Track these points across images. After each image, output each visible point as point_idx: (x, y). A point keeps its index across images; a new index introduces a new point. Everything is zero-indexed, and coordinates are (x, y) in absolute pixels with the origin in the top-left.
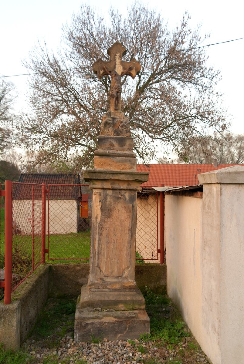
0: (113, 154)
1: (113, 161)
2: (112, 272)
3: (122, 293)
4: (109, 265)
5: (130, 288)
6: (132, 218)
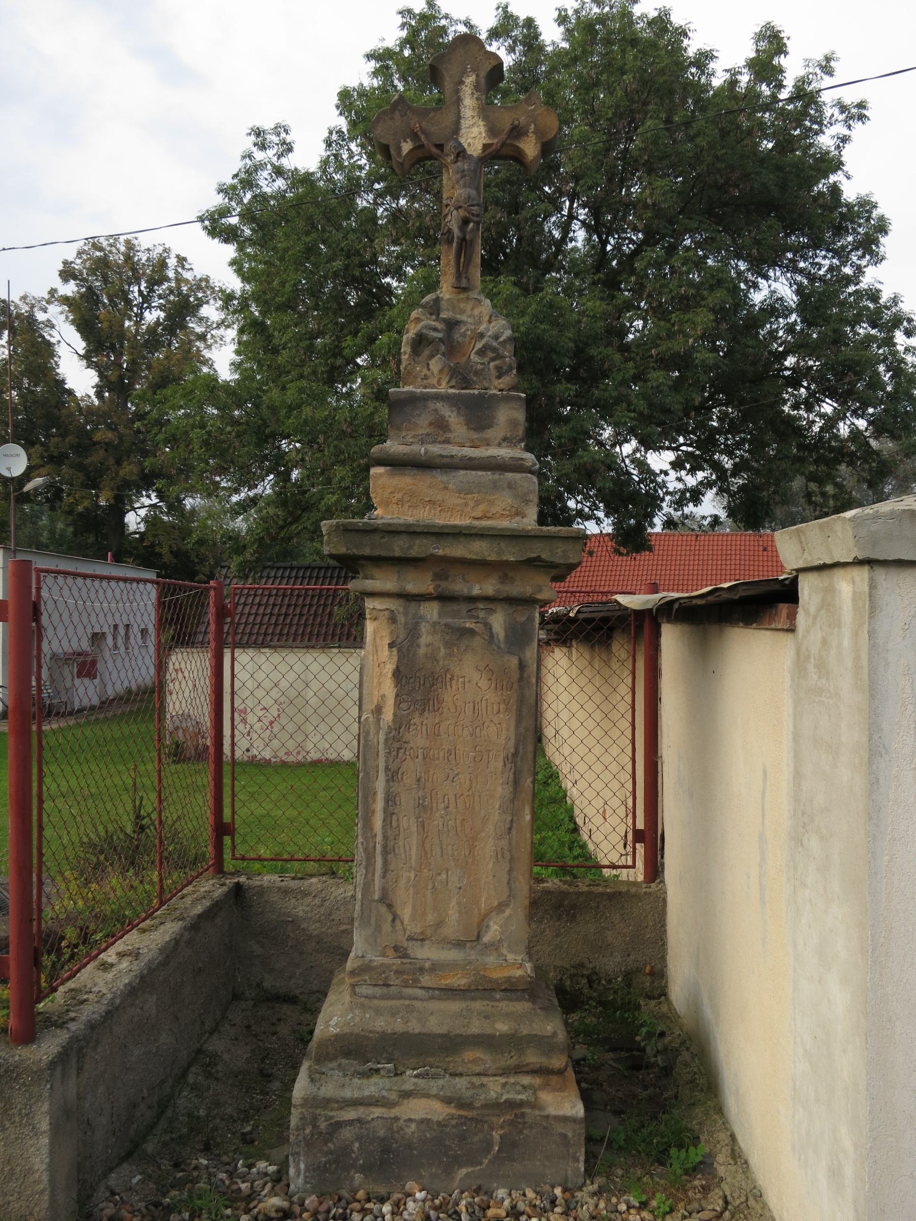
0: (445, 460)
1: (446, 488)
2: (439, 925)
3: (478, 1005)
4: (429, 896)
5: (511, 989)
6: (519, 710)
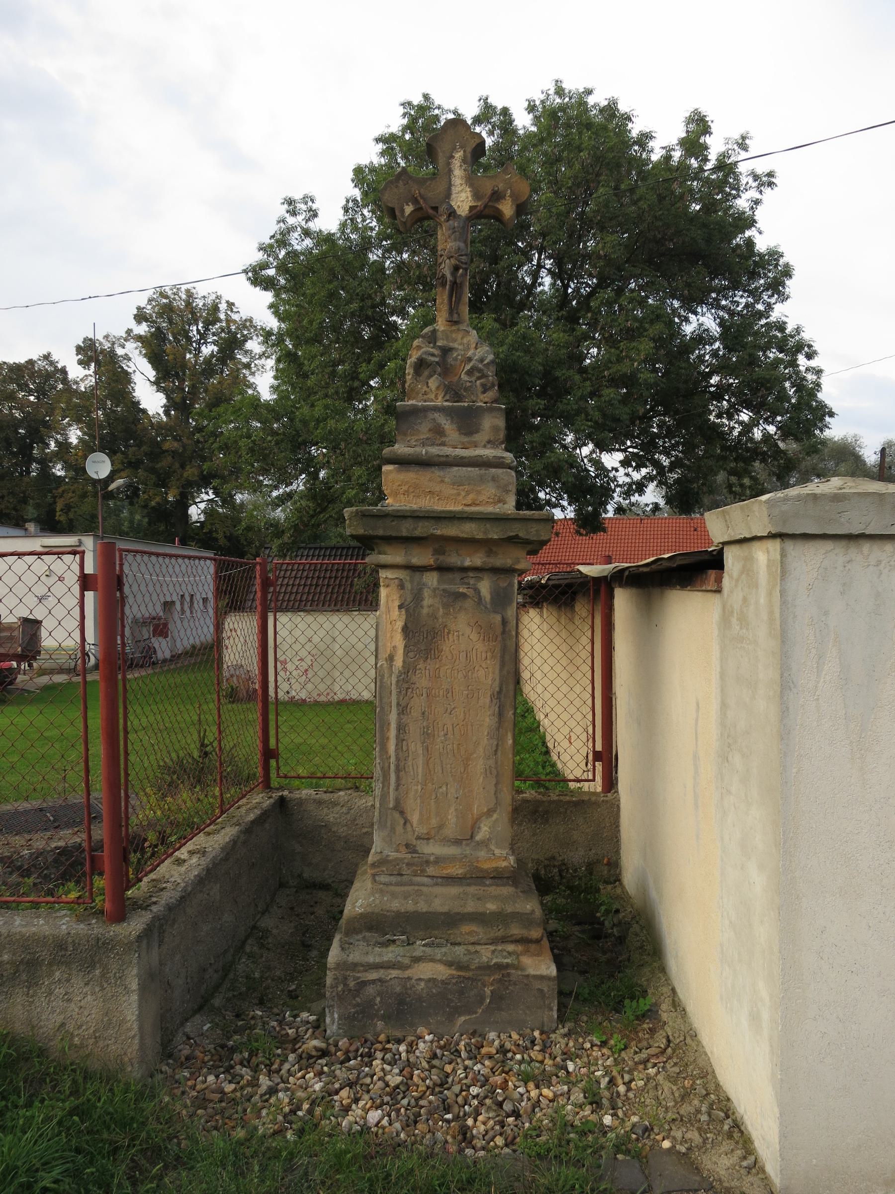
1: (442, 481)
2: (441, 827)
3: (472, 889)
4: (433, 804)
5: (498, 877)
6: (503, 657)
